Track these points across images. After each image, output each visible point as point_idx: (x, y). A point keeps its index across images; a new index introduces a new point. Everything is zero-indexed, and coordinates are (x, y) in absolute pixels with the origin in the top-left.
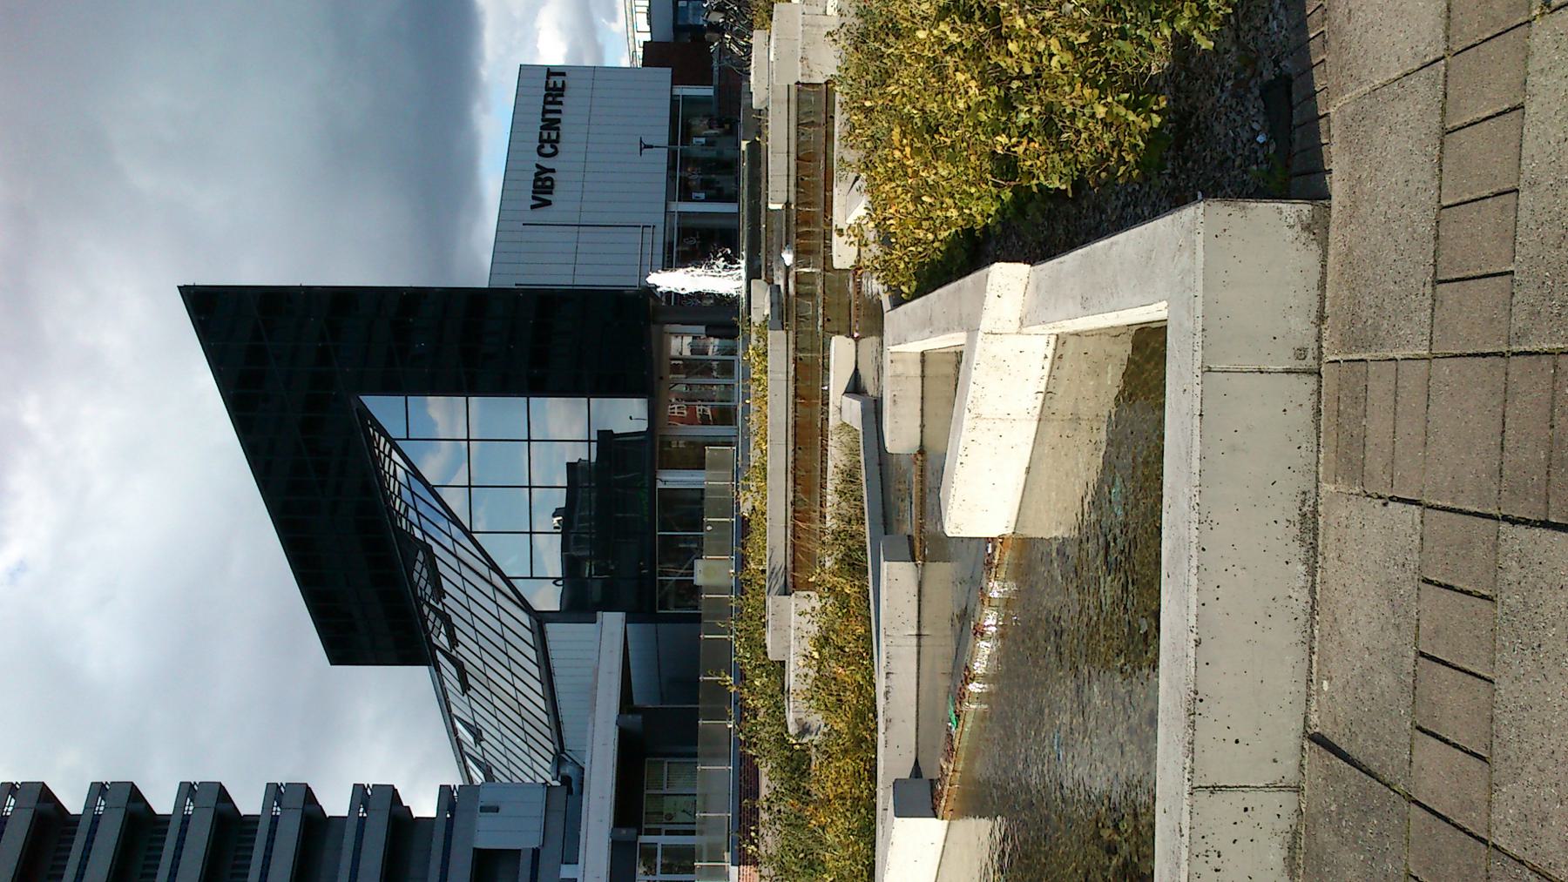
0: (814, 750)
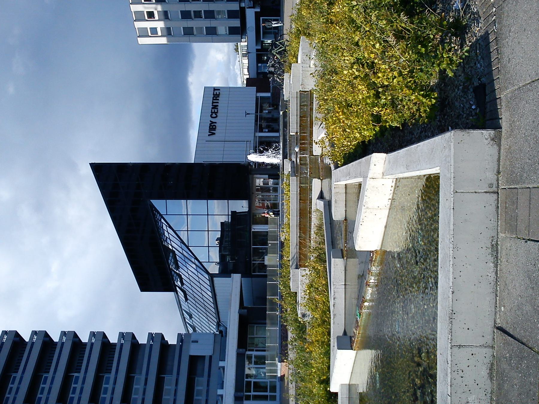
0: (308, 323)
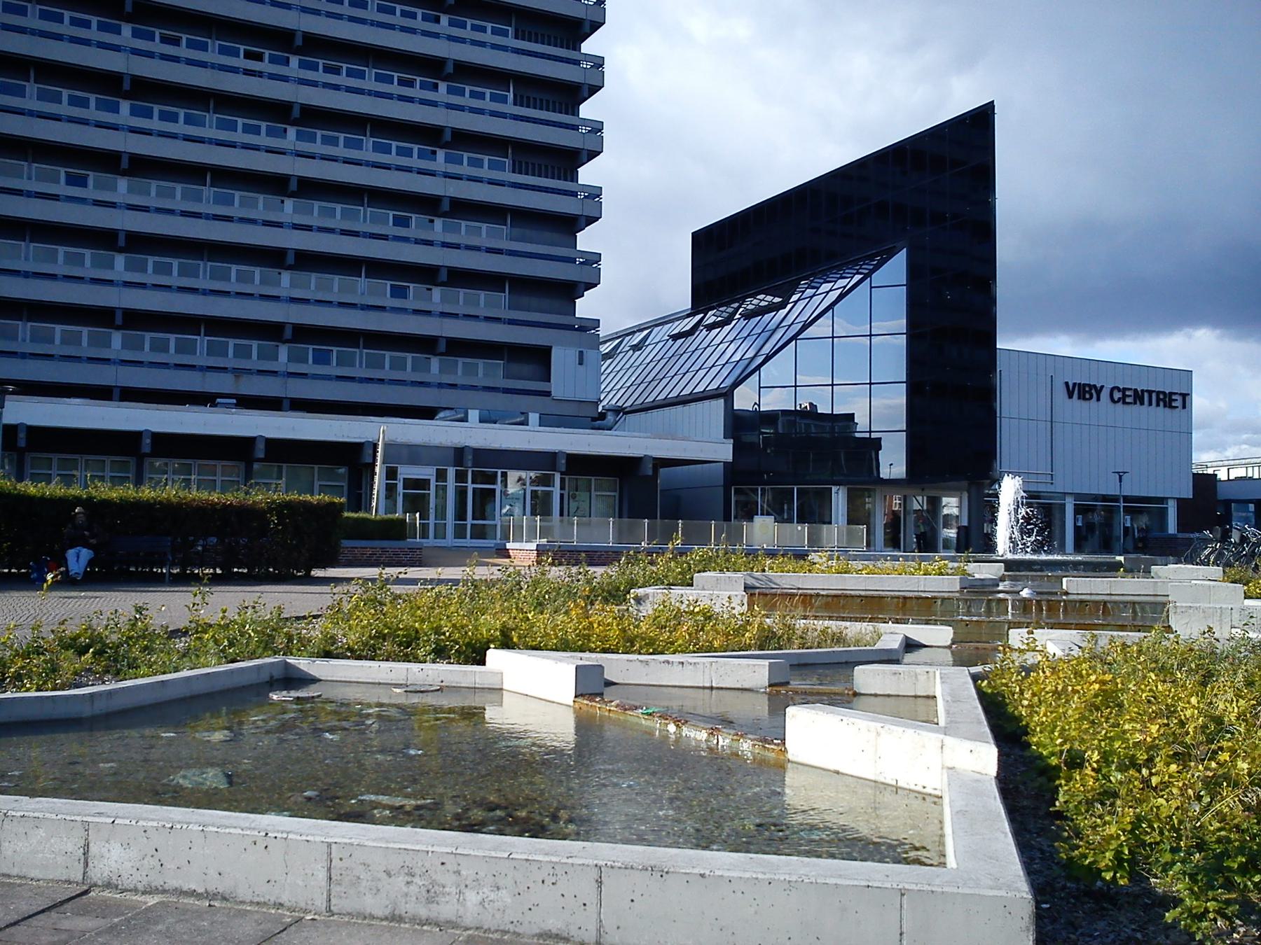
0: (625, 608)
